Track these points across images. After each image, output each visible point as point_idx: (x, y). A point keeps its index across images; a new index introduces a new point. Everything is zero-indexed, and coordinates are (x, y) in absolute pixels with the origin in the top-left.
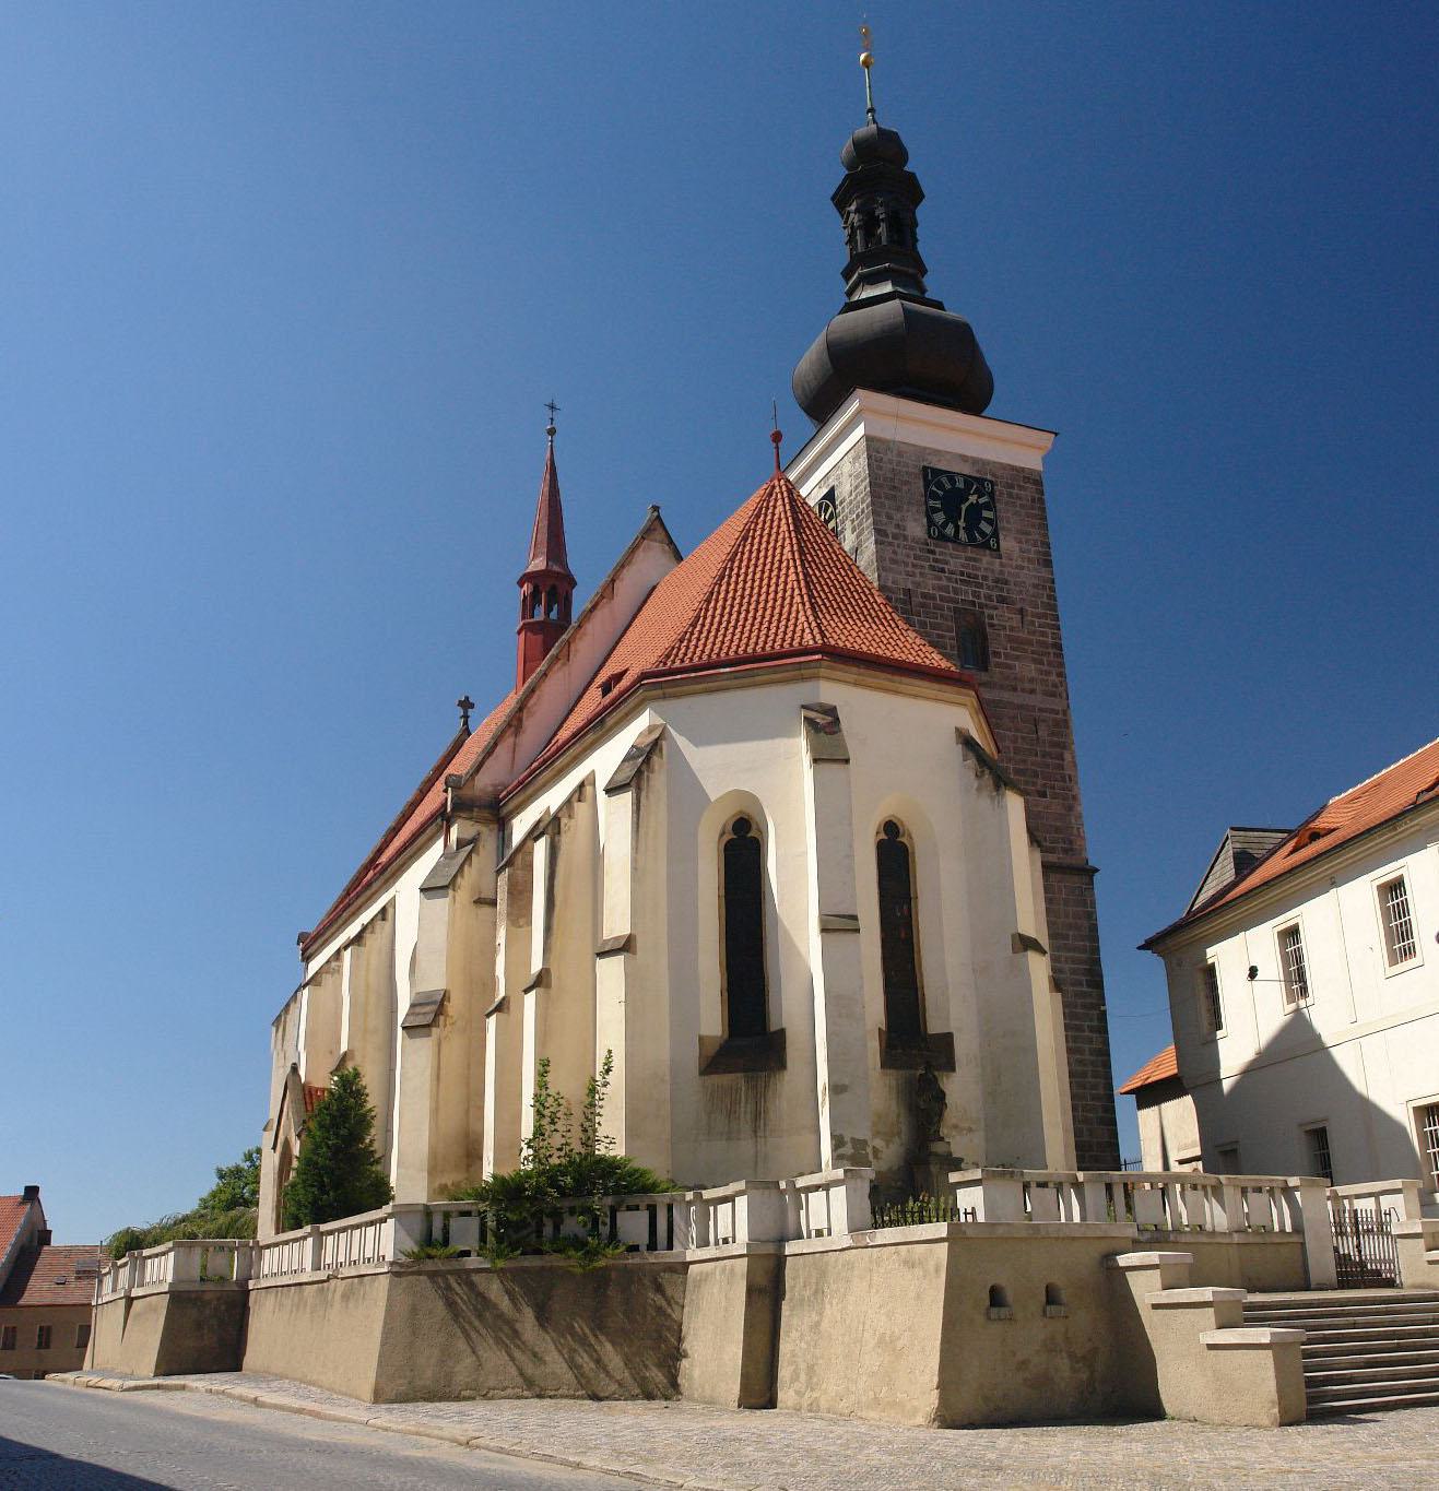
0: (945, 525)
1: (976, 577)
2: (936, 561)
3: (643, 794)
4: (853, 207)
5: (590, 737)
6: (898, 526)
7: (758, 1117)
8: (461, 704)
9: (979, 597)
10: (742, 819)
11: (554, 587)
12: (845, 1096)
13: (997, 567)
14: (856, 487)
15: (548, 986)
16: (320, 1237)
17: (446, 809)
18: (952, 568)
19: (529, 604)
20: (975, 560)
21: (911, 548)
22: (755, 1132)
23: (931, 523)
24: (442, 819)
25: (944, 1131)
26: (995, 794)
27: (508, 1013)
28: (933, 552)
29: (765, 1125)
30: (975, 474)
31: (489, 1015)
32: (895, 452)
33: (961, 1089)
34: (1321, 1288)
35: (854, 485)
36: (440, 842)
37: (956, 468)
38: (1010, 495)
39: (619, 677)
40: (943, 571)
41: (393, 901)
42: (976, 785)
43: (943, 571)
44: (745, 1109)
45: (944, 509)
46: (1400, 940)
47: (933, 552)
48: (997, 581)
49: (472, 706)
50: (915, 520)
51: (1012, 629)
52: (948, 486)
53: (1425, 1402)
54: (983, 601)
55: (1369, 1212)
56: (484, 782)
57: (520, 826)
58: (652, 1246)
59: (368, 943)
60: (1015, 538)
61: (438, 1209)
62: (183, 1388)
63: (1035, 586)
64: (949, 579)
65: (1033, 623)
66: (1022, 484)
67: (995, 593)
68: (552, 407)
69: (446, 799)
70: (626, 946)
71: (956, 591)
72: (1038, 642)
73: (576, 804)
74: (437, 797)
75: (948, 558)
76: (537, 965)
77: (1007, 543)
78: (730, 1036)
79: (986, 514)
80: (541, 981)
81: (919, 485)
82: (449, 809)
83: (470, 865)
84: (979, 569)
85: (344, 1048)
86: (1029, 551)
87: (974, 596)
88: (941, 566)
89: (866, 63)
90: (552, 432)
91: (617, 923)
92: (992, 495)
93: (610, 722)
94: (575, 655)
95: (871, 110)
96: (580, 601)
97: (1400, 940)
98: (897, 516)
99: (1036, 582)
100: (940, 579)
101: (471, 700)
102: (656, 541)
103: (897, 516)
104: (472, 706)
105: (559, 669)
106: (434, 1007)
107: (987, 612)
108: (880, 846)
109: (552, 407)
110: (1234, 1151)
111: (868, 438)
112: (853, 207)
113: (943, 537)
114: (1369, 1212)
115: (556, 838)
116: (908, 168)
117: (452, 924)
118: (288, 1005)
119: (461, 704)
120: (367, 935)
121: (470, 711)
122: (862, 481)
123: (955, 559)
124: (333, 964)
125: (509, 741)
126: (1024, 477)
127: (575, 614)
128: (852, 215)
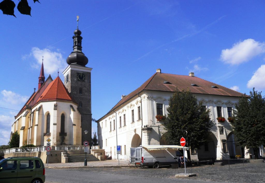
12: (54, 139)
16: (9, 150)
19: (40, 80)
23: (77, 79)
24: (26, 109)
33: (67, 138)
34: (88, 154)
36: (25, 111)
37: (81, 72)
39: (42, 96)
45: (79, 77)
49: (36, 89)
52: (79, 75)
53: (40, 154)
56: (30, 105)
57: (33, 110)
58: (34, 151)
67: (84, 86)
68: (43, 57)
70: (37, 125)
74: (26, 107)
76: (31, 126)
77: (86, 81)
79: (84, 77)
80: (32, 127)
81: (76, 74)
85: (17, 130)
89: (78, 21)
90: (43, 60)
91: (36, 123)
92: (85, 75)
95: (78, 27)
96: (45, 80)
103: (73, 78)
104: (36, 89)
109: (43, 57)
111: (71, 70)
113: (78, 80)
116: (81, 35)
117: (26, 120)
120: (19, 119)
123: (80, 83)
125: (32, 101)
127: (45, 81)
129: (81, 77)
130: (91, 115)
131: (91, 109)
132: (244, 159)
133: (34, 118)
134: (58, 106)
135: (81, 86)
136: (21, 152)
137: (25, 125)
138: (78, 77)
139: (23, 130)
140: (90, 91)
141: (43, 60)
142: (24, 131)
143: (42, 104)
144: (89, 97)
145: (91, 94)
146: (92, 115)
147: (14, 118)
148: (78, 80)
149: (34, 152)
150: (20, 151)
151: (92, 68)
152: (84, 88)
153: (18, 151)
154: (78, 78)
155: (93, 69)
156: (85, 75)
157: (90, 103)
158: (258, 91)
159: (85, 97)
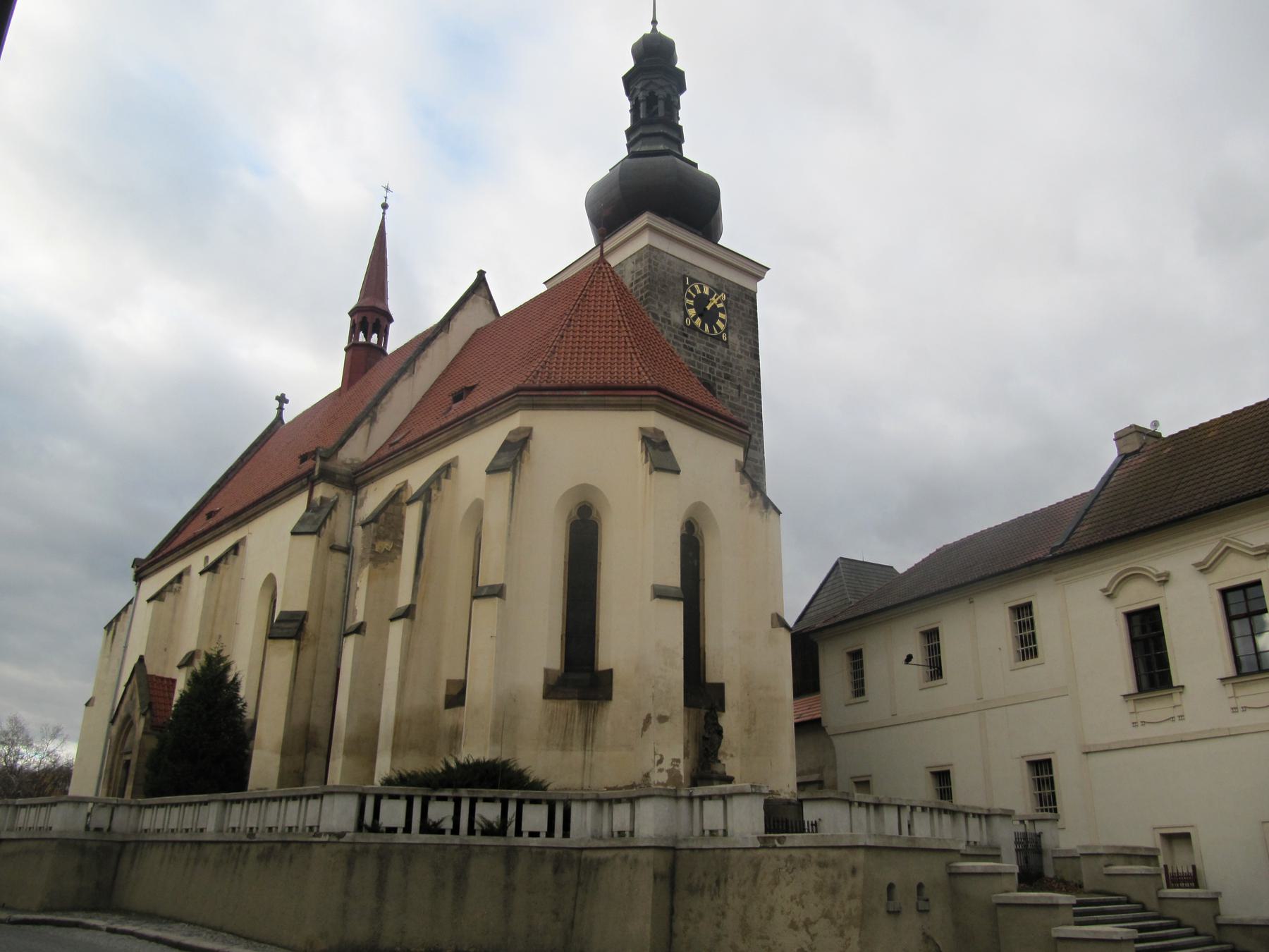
0: (695, 318)
1: (712, 358)
2: (687, 342)
3: (517, 478)
4: (639, 87)
5: (458, 430)
6: (665, 313)
7: (588, 736)
8: (277, 398)
9: (713, 373)
10: (585, 506)
11: (378, 321)
13: (726, 354)
14: (637, 281)
15: (413, 618)
17: (313, 473)
18: (698, 349)
20: (712, 346)
21: (673, 331)
22: (585, 745)
25: (720, 758)
26: (764, 511)
27: (364, 635)
28: (686, 336)
29: (593, 741)
30: (716, 287)
31: (346, 635)
32: (667, 261)
35: (635, 279)
36: (305, 496)
38: (737, 305)
40: (692, 350)
41: (243, 540)
42: (749, 502)
43: (692, 350)
44: (578, 727)
45: (696, 307)
46: (1027, 647)
47: (686, 336)
48: (725, 363)
49: (287, 401)
50: (677, 311)
51: (732, 398)
52: (699, 291)
54: (715, 375)
55: (793, 823)
58: (550, 833)
59: (221, 572)
60: (738, 336)
61: (371, 792)
62: (77, 925)
63: (748, 371)
64: (695, 356)
65: (745, 396)
66: (744, 299)
67: (723, 372)
68: (387, 189)
69: (315, 465)
71: (700, 366)
72: (749, 411)
73: (443, 481)
75: (696, 342)
78: (566, 671)
79: (721, 315)
80: (408, 613)
82: (316, 474)
83: (330, 519)
84: (714, 353)
86: (745, 346)
87: (710, 371)
88: (691, 346)
90: (385, 206)
93: (479, 419)
94: (418, 370)
97: (1027, 647)
98: (665, 306)
99: (749, 368)
100: (690, 355)
101: (287, 397)
102: (480, 295)
103: (665, 306)
104: (287, 401)
105: (406, 379)
106: (296, 625)
107: (718, 384)
108: (683, 537)
109: (387, 189)
110: (867, 783)
112: (639, 87)
114: (793, 823)
115: (428, 505)
118: (119, 615)
119: (277, 398)
120: (222, 565)
121: (285, 406)
122: (643, 278)
124: (176, 585)
126: (746, 295)
128: (638, 92)
129: (709, 307)
133: (427, 538)
136: (416, 837)
137: (310, 601)
138: (691, 302)
139: (294, 642)
140: (760, 415)
141: (385, 206)
142: (298, 650)
143: (527, 424)
147: (132, 572)
148: (693, 327)
149: (550, 842)
150: (400, 822)
151: (768, 269)
153: (386, 820)
154: (692, 312)
155: (768, 273)
158: (414, 769)
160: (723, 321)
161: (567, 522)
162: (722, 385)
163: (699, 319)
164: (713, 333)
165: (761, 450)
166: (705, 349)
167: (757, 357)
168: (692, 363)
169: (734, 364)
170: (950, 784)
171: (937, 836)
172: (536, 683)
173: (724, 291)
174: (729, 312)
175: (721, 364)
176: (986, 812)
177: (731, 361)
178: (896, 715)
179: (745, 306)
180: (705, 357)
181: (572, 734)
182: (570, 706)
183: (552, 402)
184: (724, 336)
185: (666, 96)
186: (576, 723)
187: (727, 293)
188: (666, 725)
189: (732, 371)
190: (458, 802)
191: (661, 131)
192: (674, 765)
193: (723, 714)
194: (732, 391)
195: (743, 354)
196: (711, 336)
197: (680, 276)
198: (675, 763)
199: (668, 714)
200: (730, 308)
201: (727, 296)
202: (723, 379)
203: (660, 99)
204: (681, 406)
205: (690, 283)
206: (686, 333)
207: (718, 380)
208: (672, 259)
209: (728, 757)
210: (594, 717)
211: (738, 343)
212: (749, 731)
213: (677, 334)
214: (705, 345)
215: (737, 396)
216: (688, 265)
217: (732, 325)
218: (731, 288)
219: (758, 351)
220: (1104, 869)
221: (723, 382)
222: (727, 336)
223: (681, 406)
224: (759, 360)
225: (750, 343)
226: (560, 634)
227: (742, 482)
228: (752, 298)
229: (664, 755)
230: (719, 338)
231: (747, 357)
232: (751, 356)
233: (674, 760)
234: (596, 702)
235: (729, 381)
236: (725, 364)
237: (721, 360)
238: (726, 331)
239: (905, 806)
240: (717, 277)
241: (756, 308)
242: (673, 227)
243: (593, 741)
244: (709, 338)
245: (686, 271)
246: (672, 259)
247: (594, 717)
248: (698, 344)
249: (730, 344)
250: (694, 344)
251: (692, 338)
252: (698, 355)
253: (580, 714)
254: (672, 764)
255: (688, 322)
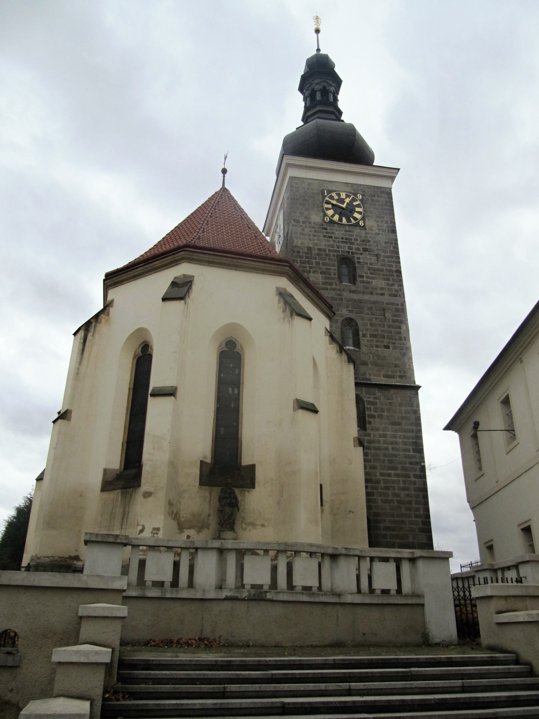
0: (333, 216)
1: (351, 240)
20: (350, 231)
21: (314, 227)
22: (122, 525)
28: (326, 229)
38: (373, 200)
47: (326, 229)
48: (363, 241)
63: (386, 243)
64: (334, 241)
65: (384, 260)
66: (379, 194)
67: (361, 247)
79: (357, 209)
90: (224, 171)
130: (417, 394)
131: (411, 358)
132: (262, 590)
134: (196, 288)
135: (345, 247)
141: (224, 171)
142: (356, 593)
144: (393, 300)
145: (401, 285)
146: (420, 391)
148: (332, 222)
152: (365, 258)
154: (330, 212)
156: (361, 200)
157: (403, 327)
159: (374, 298)
160: (360, 213)
161: (134, 358)
162: (361, 256)
163: (344, 219)
164: (351, 222)
165: (402, 296)
166: (343, 234)
167: (394, 231)
168: (333, 246)
169: (372, 240)
170: (533, 541)
171: (406, 587)
172: (97, 480)
173: (360, 192)
174: (365, 205)
175: (359, 242)
176: (330, 551)
177: (369, 239)
178: (498, 481)
179: (380, 199)
180: (344, 240)
181: (115, 518)
182: (115, 495)
183: (123, 278)
184: (361, 223)
185: (322, 88)
186: (118, 509)
187: (363, 193)
188: (150, 499)
189: (370, 246)
190: (290, 586)
191: (318, 109)
192: (154, 533)
193: (254, 490)
194: (371, 259)
195: (381, 232)
196: (349, 225)
197: (319, 191)
198: (155, 532)
199: (152, 490)
200: (366, 203)
201: (363, 195)
202: (362, 252)
203: (317, 91)
204: (210, 254)
205: (328, 194)
206: (325, 227)
207: (356, 253)
208: (311, 181)
209: (258, 527)
210: (129, 501)
211: (375, 225)
212: (279, 503)
213: (317, 229)
214: (343, 232)
215: (376, 262)
216: (326, 182)
217: (369, 214)
218: (366, 190)
219: (395, 227)
220: (495, 616)
221: (361, 254)
222: (364, 222)
223: (210, 254)
224: (396, 233)
225: (387, 222)
226: (121, 441)
227: (279, 302)
228: (388, 193)
229: (145, 526)
230: (357, 225)
231: (384, 233)
232: (388, 232)
233: (154, 529)
234: (132, 489)
235: (368, 253)
236: (363, 242)
237: (359, 239)
238: (363, 219)
239: (364, 557)
240: (352, 185)
241: (392, 198)
242: (306, 160)
243: (127, 522)
244: (347, 226)
245: (325, 186)
246: (311, 181)
247: (129, 501)
248: (337, 233)
249: (367, 227)
250: (333, 233)
251: (330, 229)
252: (337, 240)
253: (121, 500)
254: (152, 532)
255: (327, 219)
